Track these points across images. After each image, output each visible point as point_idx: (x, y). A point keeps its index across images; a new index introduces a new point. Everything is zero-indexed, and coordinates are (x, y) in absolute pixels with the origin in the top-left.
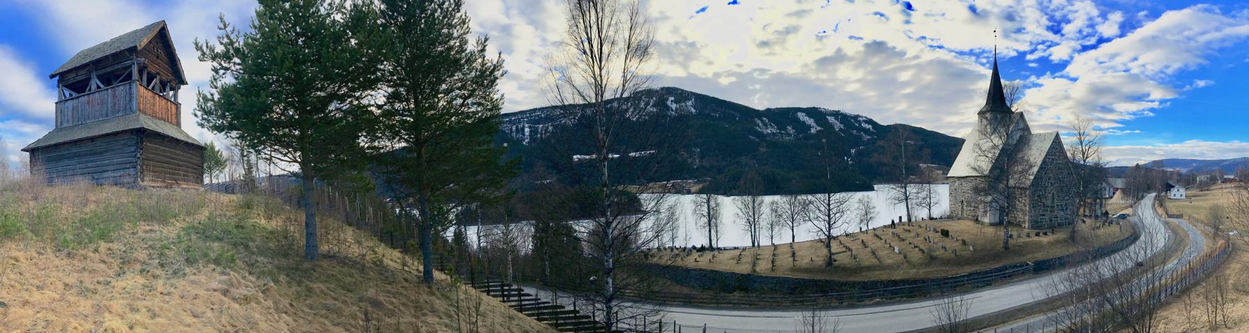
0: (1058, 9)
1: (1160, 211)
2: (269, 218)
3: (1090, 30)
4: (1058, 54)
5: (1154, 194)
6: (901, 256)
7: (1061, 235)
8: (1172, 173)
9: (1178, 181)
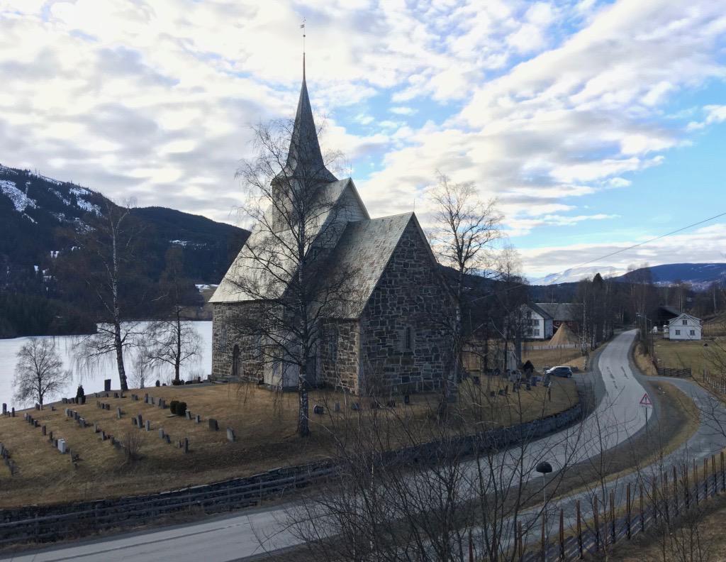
0: (440, 13)
1: (644, 362)
2: (537, 322)
3: (496, 44)
4: (446, 86)
5: (634, 332)
6: (69, 457)
7: (419, 407)
8: (673, 290)
9: (687, 307)
